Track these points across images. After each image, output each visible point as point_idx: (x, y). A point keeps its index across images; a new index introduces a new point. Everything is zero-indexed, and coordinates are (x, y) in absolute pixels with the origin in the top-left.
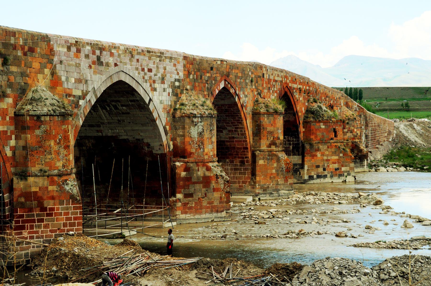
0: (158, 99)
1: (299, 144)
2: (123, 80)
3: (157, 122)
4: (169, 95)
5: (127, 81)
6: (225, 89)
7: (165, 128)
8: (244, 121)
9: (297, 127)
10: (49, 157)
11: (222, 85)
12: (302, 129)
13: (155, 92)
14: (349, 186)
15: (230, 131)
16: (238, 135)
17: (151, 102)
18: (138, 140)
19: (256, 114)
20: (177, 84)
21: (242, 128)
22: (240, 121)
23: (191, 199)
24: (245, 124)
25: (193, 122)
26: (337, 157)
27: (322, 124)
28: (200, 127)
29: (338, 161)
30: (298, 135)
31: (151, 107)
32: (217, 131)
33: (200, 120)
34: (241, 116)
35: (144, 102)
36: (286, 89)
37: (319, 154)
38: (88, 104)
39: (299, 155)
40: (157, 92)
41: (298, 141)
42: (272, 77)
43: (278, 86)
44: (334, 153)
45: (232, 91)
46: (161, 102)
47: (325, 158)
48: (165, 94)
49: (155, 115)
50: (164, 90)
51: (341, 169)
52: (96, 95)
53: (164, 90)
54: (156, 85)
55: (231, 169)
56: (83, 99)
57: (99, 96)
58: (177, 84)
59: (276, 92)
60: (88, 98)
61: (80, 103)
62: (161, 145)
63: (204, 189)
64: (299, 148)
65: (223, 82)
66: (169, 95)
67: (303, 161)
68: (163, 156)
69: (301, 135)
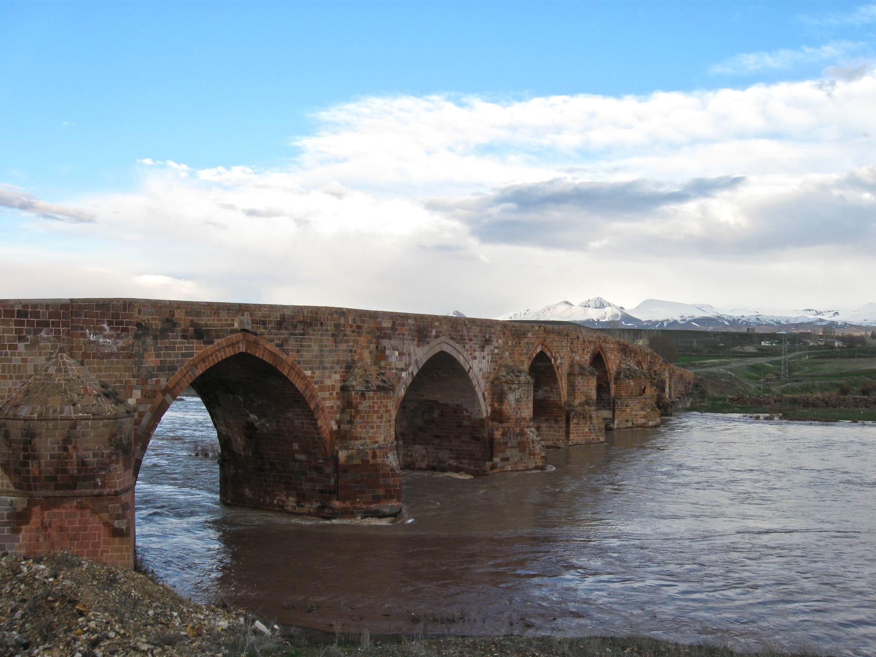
0: (478, 366)
1: (610, 400)
2: (445, 350)
3: (476, 389)
4: (488, 362)
5: (448, 351)
6: (541, 352)
7: (483, 394)
8: (560, 382)
9: (608, 384)
10: (371, 431)
11: (539, 350)
12: (613, 386)
13: (475, 360)
14: (691, 207)
15: (545, 391)
16: (554, 394)
17: (471, 370)
18: (458, 405)
19: (571, 374)
20: (496, 351)
21: (557, 388)
22: (555, 380)
23: (507, 463)
24: (561, 385)
25: (511, 388)
26: (644, 413)
27: (632, 381)
28: (518, 394)
29: (645, 417)
30: (609, 391)
31: (471, 375)
32: (534, 390)
33: (517, 387)
34: (556, 377)
35: (464, 371)
36: (600, 350)
37: (628, 410)
38: (410, 376)
39: (610, 410)
40: (477, 361)
41: (609, 396)
42: (586, 339)
43: (592, 347)
44: (642, 409)
45: (548, 354)
46: (480, 370)
47: (634, 413)
48: (484, 361)
49: (475, 382)
50: (484, 358)
51: (648, 423)
52: (418, 367)
53: (484, 358)
54: (477, 354)
55: (546, 427)
56: (406, 371)
57: (420, 367)
58: (496, 351)
59: (590, 352)
60: (410, 370)
61: (403, 375)
62: (479, 411)
63: (520, 454)
64: (610, 403)
65: (540, 347)
66: (488, 362)
67: (614, 415)
68: (482, 420)
69: (613, 392)
